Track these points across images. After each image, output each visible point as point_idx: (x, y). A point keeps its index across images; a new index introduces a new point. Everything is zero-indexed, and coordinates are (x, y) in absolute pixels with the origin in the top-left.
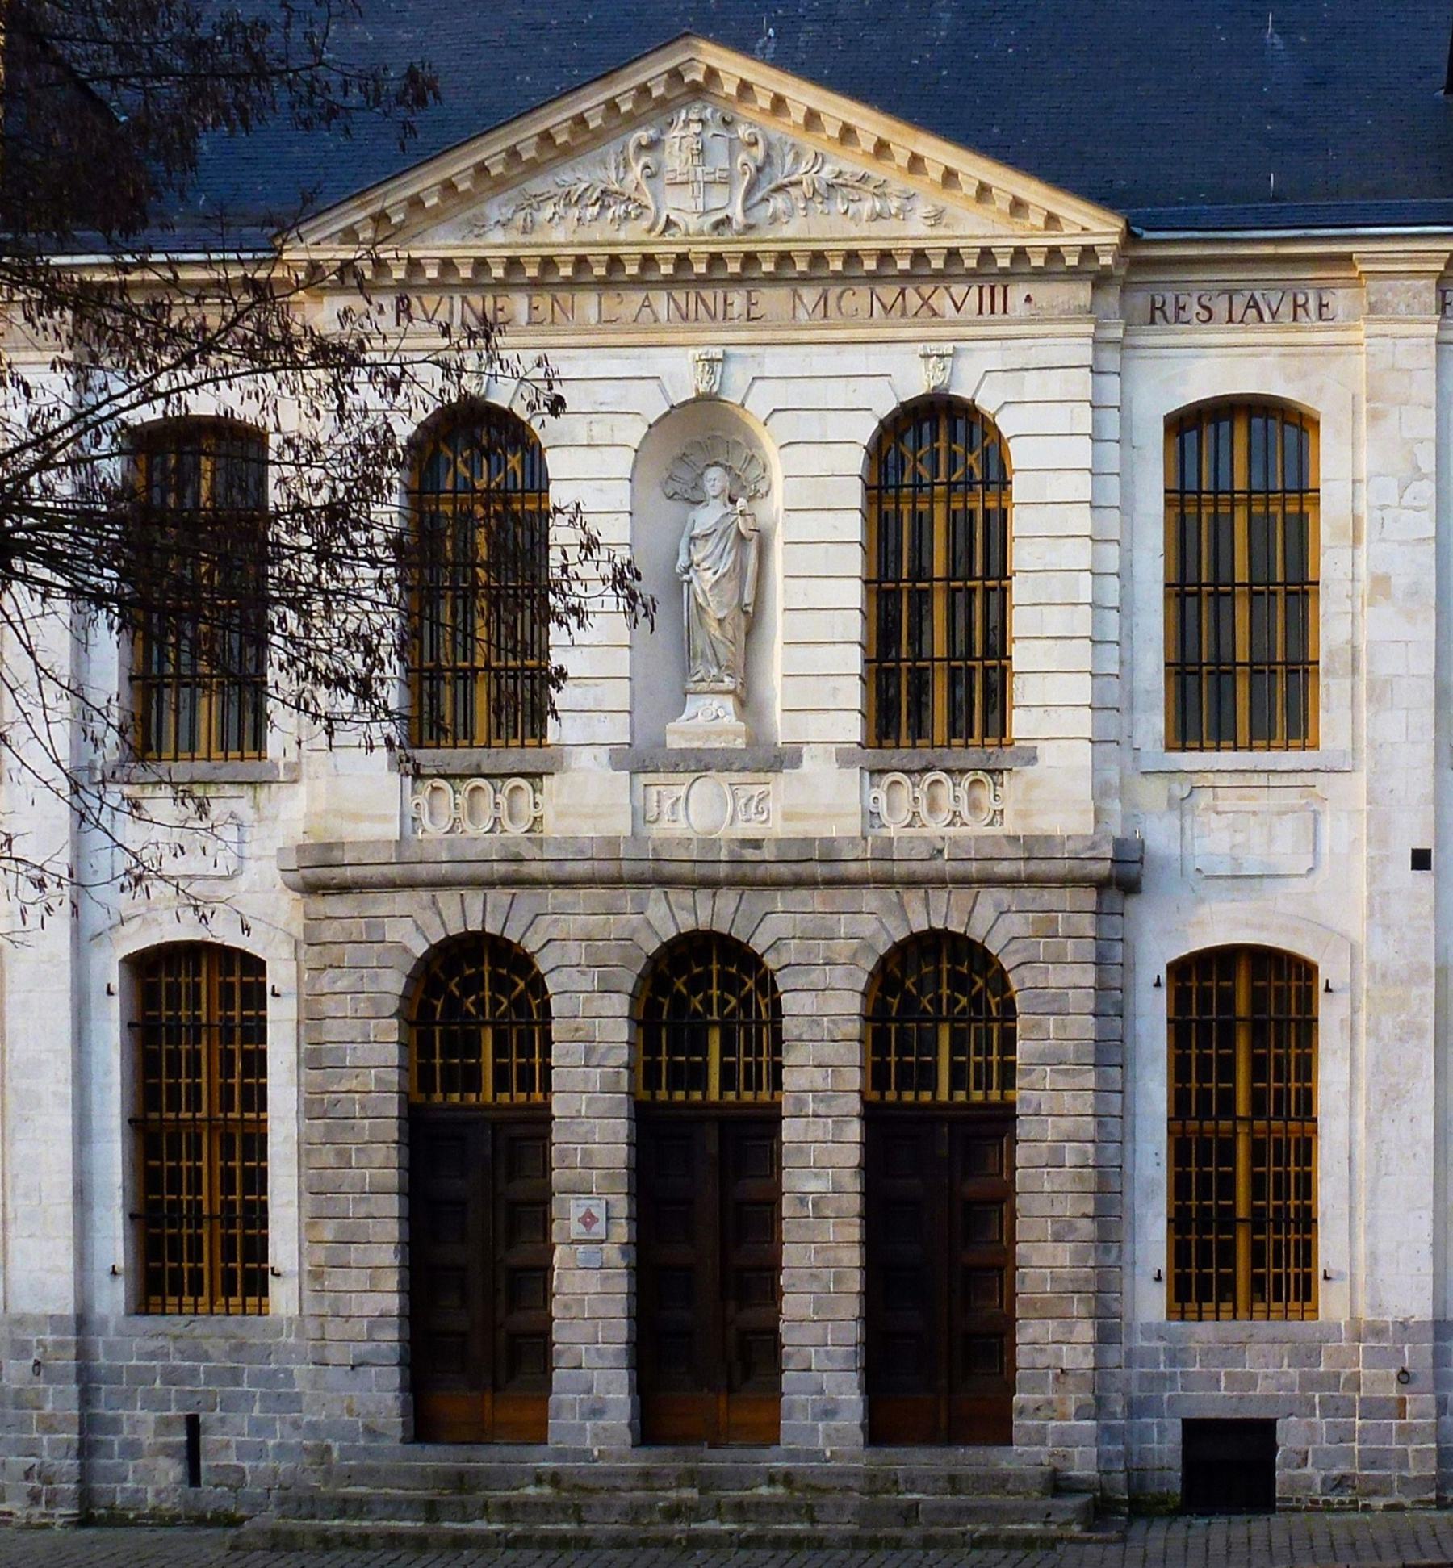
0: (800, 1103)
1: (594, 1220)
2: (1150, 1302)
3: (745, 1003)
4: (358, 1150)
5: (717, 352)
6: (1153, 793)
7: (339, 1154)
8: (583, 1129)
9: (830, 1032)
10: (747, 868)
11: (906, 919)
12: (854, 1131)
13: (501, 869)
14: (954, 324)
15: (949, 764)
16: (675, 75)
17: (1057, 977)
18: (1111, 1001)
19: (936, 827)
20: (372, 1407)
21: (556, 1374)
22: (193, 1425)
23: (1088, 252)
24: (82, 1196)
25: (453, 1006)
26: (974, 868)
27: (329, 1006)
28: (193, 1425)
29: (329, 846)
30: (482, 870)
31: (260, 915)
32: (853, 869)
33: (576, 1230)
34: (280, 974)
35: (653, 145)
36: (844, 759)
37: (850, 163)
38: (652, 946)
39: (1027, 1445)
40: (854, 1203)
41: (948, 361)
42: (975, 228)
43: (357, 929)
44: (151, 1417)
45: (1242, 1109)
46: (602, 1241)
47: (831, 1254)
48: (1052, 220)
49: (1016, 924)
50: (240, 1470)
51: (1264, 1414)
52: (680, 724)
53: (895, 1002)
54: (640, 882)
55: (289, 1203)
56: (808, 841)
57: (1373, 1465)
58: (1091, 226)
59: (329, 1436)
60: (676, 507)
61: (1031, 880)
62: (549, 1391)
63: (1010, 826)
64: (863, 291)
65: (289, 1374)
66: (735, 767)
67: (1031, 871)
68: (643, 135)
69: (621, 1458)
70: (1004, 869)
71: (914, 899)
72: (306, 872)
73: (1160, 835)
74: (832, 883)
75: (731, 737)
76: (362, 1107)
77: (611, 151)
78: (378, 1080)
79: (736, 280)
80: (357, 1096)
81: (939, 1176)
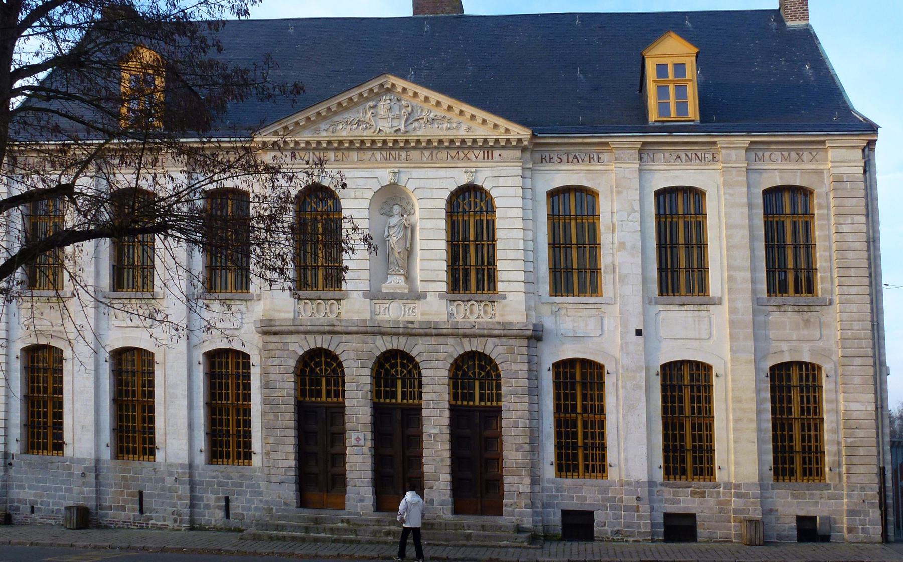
0: (429, 404)
2: (549, 472)
3: (409, 372)
5: (396, 170)
6: (546, 310)
7: (275, 416)
11: (463, 347)
12: (447, 414)
13: (327, 328)
16: (382, 86)
17: (514, 367)
18: (533, 375)
19: (473, 318)
22: (227, 500)
23: (519, 141)
24: (190, 426)
28: (227, 500)
29: (271, 320)
30: (321, 329)
31: (248, 340)
32: (445, 331)
33: (354, 442)
34: (255, 359)
35: (374, 107)
36: (441, 296)
37: (440, 113)
38: (378, 354)
40: (448, 437)
42: (481, 133)
43: (280, 346)
44: (213, 497)
48: (507, 131)
49: (501, 350)
50: (243, 515)
51: (590, 509)
52: (386, 284)
53: (460, 373)
54: (373, 333)
56: (429, 322)
57: (628, 527)
58: (520, 133)
60: (384, 217)
61: (505, 336)
63: (497, 318)
64: (445, 152)
67: (505, 333)
68: (371, 104)
70: (496, 332)
71: (465, 341)
73: (548, 322)
77: (361, 108)
79: (403, 148)
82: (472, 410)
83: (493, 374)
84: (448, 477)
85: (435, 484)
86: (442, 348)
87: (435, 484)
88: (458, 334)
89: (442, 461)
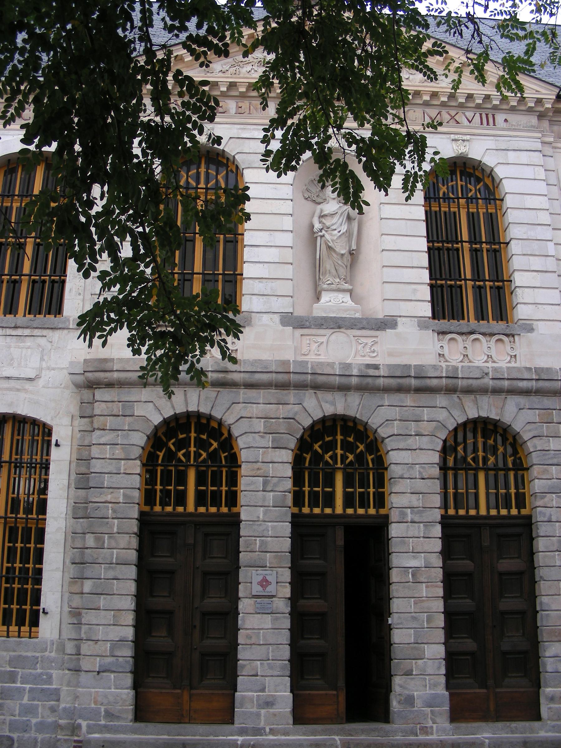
0: (404, 514)
1: (268, 583)
4: (109, 537)
7: (97, 539)
8: (261, 528)
9: (420, 472)
10: (369, 380)
12: (437, 530)
14: (503, 129)
15: (482, 330)
20: (111, 699)
21: (240, 679)
23: (539, 101)
25: (170, 456)
26: (506, 383)
27: (95, 452)
32: (435, 382)
33: (257, 589)
34: (63, 432)
36: (422, 324)
38: (307, 422)
39: (557, 720)
40: (439, 574)
41: (466, 143)
43: (117, 408)
45: (17, 579)
46: (273, 596)
47: (425, 604)
50: (11, 739)
54: (301, 386)
55: (57, 569)
56: (408, 367)
59: (80, 717)
60: (309, 204)
61: (538, 392)
62: (235, 690)
65: (50, 677)
66: (358, 327)
69: (286, 733)
71: (468, 401)
72: (89, 375)
74: (419, 390)
75: (353, 312)
76: (114, 511)
78: (125, 495)
80: (110, 505)
81: (343, 566)
82: (477, 524)
83: (370, 458)
84: (440, 651)
85: (416, 666)
86: (426, 414)
87: (416, 666)
88: (454, 387)
89: (429, 620)
